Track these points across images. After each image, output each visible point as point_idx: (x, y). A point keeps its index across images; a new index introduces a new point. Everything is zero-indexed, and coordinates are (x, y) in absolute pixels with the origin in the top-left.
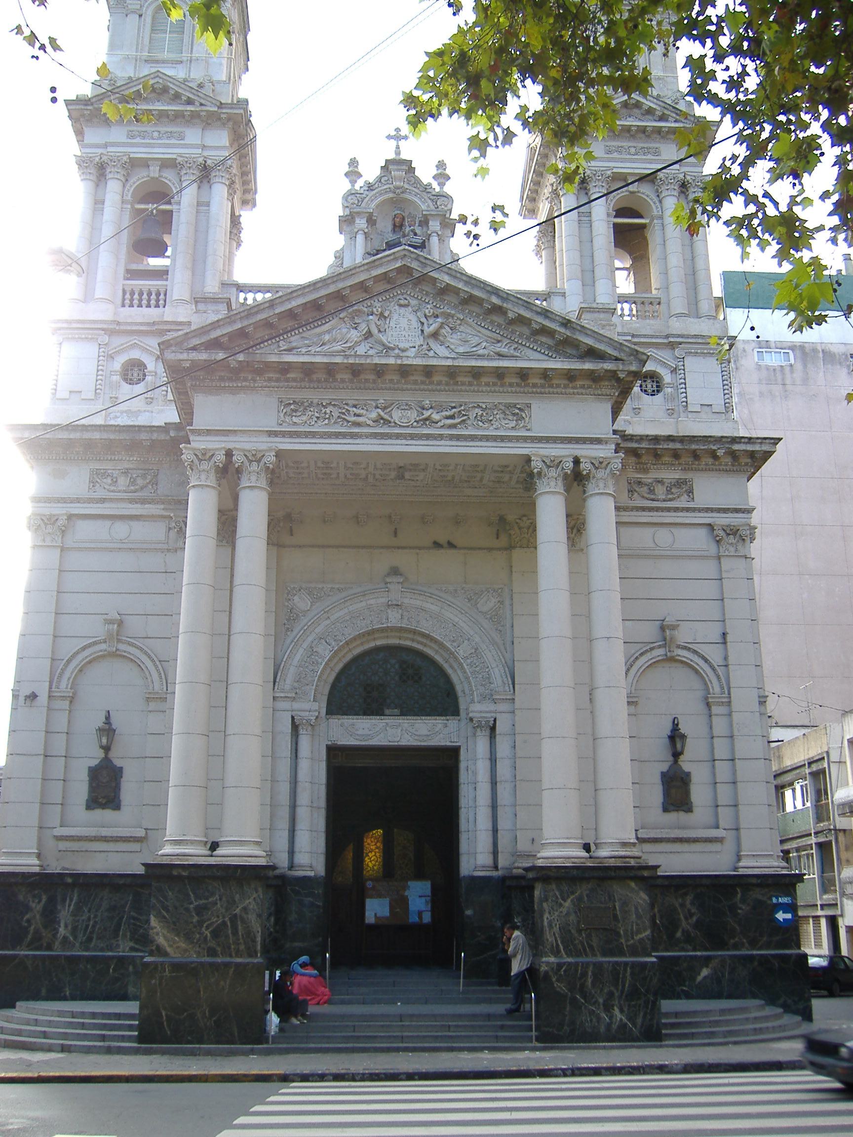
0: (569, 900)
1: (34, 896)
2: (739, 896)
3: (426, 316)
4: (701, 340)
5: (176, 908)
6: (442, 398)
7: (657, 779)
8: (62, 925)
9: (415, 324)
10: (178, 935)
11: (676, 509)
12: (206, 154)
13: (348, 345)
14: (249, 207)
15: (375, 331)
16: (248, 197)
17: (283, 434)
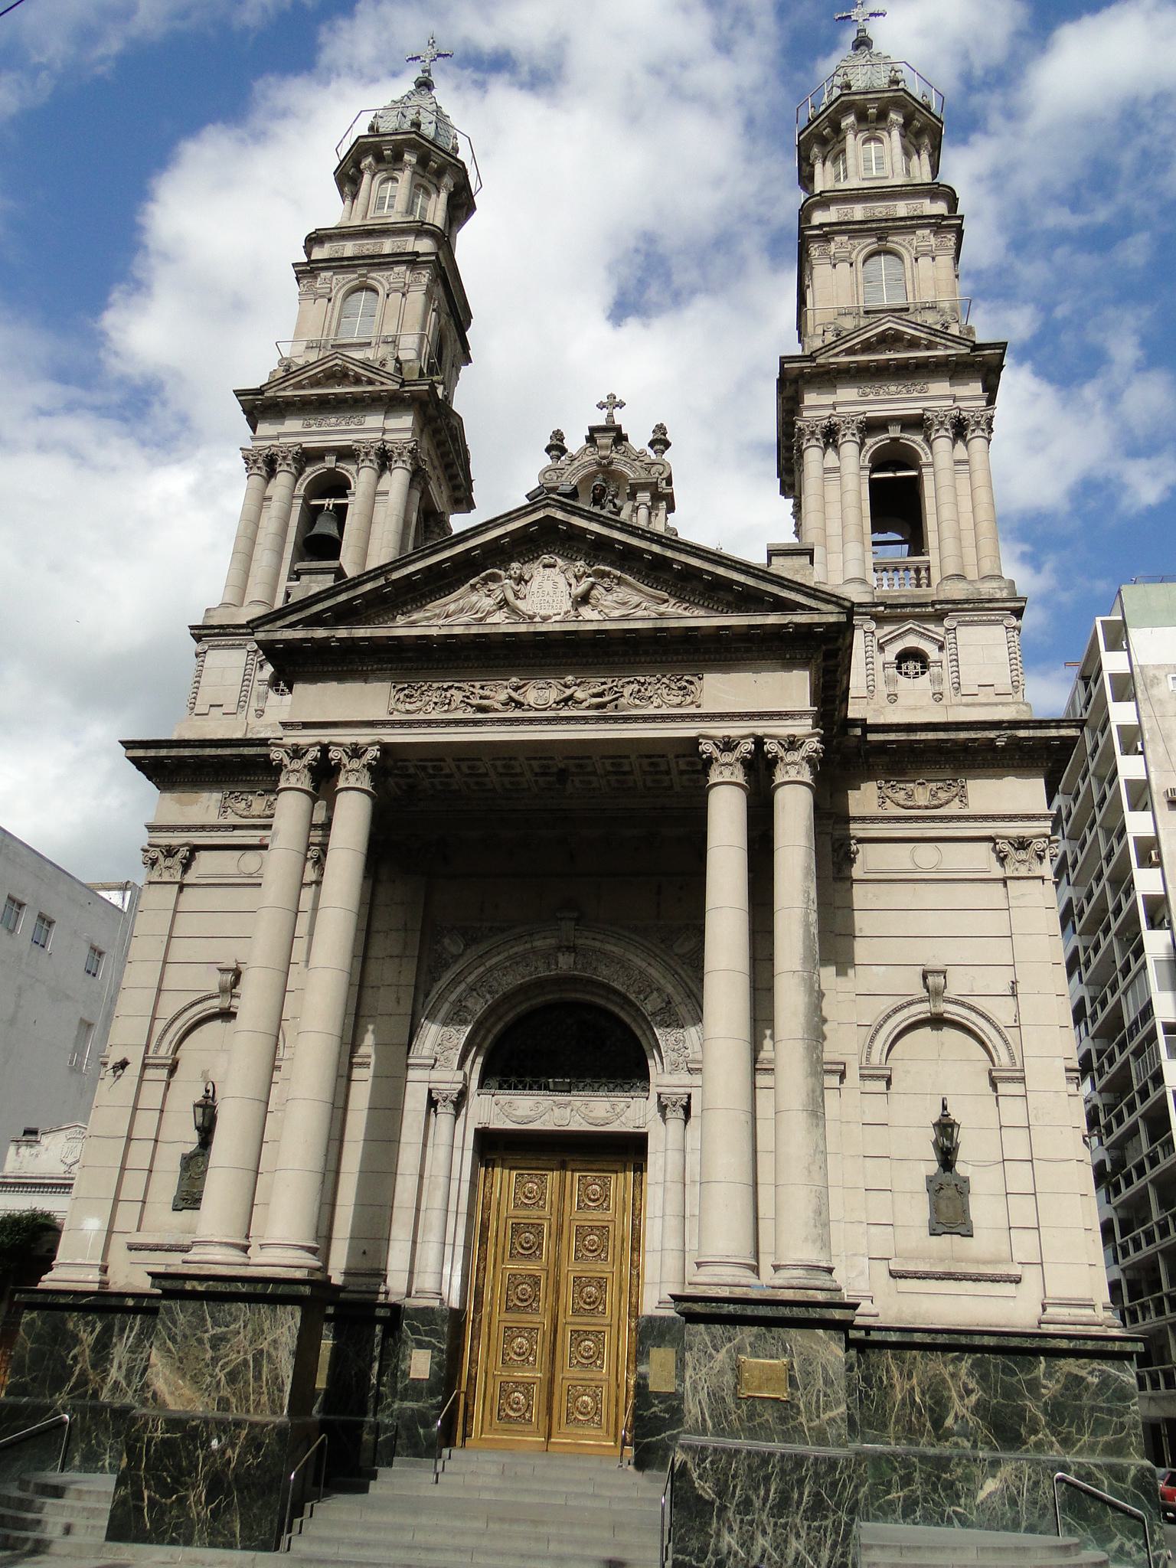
0: (724, 1350)
1: (87, 1324)
2: (1043, 1366)
5: (185, 1336)
7: (922, 1185)
8: (115, 1364)
10: (183, 1377)
12: (386, 437)
13: (479, 615)
15: (511, 597)
16: (460, 494)
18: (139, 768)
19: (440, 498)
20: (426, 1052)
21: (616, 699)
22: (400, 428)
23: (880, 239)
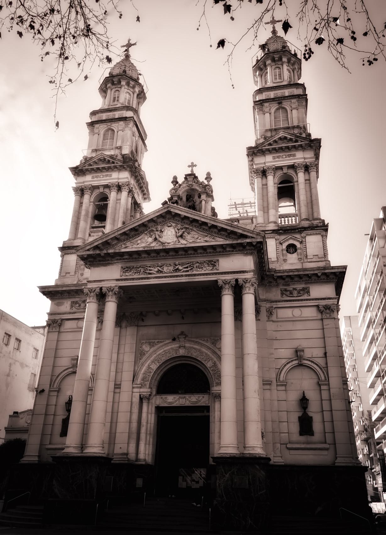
3: (178, 230)
6: (184, 261)
9: (174, 233)
11: (302, 300)
12: (119, 181)
14: (147, 200)
15: (157, 237)
16: (145, 196)
17: (122, 280)
20: (138, 383)
22: (124, 176)
23: (279, 103)
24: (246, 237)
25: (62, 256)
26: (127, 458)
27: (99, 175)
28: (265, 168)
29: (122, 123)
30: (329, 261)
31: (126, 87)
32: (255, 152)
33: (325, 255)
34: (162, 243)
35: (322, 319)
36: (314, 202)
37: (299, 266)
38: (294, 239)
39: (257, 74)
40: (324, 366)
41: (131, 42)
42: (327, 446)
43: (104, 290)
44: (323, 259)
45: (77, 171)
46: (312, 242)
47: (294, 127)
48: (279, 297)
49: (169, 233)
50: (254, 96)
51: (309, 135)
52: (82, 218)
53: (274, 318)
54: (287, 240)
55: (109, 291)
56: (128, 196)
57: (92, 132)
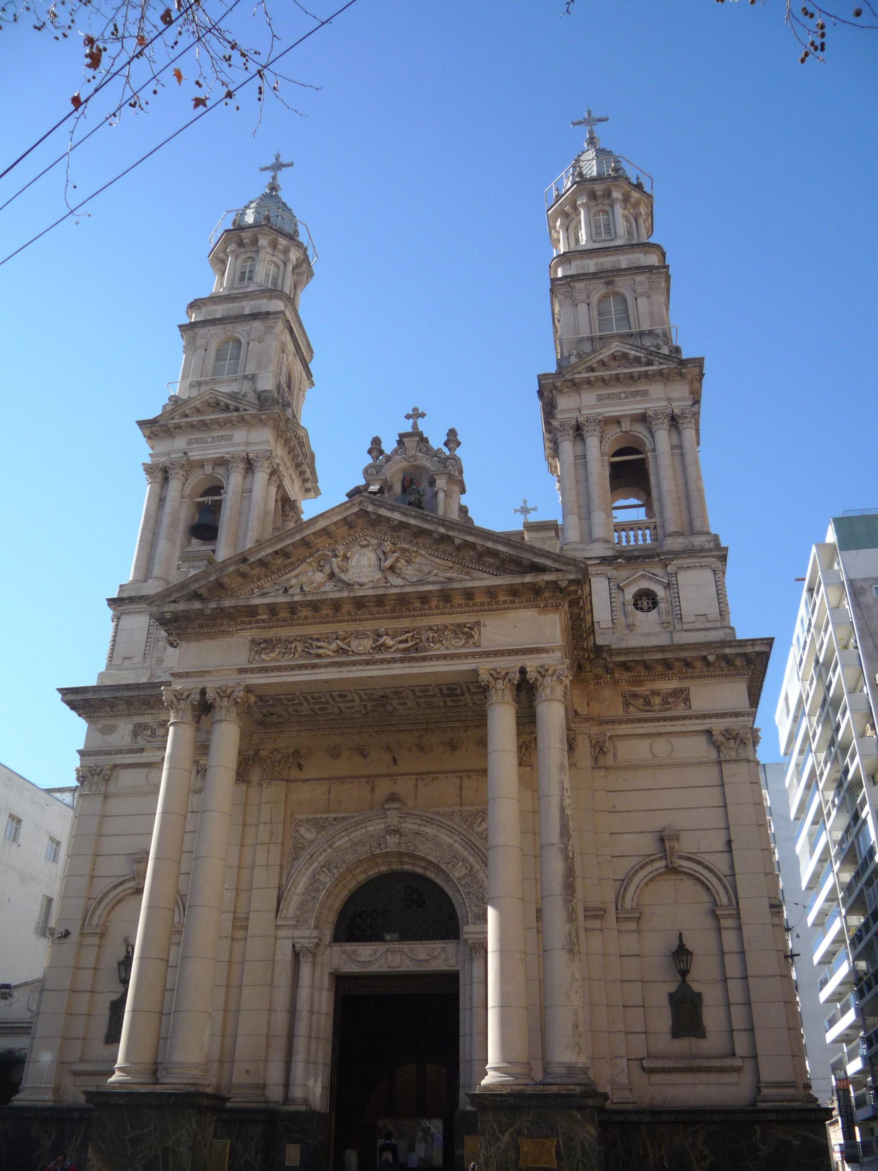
0: (508, 1134)
2: (758, 1134)
3: (384, 553)
4: (691, 552)
7: (665, 1001)
14: (312, 494)
15: (336, 570)
16: (309, 485)
18: (72, 709)
19: (293, 490)
21: (416, 643)
22: (261, 439)
23: (607, 284)
24: (543, 569)
25: (117, 618)
26: (263, 1095)
27: (204, 435)
28: (580, 420)
29: (257, 324)
30: (732, 629)
31: (269, 250)
32: (558, 384)
33: (723, 613)
34: (349, 585)
35: (720, 763)
36: (694, 495)
37: (663, 640)
38: (651, 579)
39: (558, 223)
40: (728, 871)
41: (281, 160)
42: (738, 1062)
43: (210, 695)
44: (719, 624)
45: (153, 429)
46: (693, 585)
47: (641, 334)
48: (618, 710)
49: (364, 561)
50: (552, 269)
51: (678, 350)
52: (163, 532)
53: (609, 760)
54: (635, 581)
55: (222, 698)
56: (269, 484)
57: (190, 346)
